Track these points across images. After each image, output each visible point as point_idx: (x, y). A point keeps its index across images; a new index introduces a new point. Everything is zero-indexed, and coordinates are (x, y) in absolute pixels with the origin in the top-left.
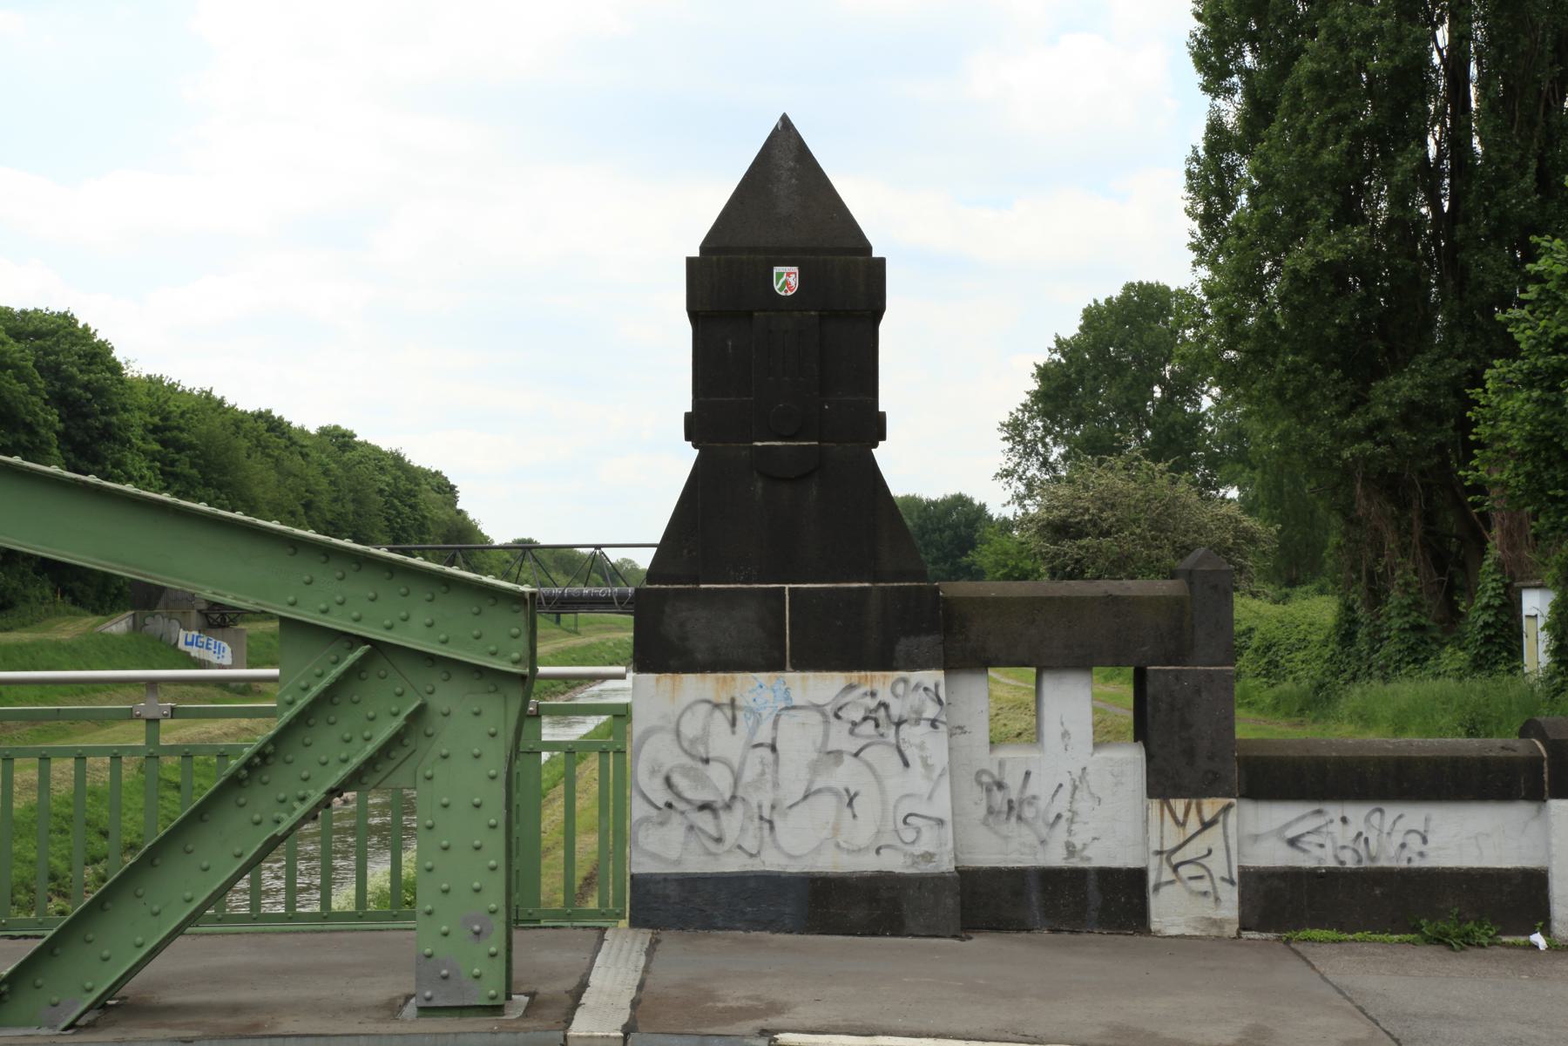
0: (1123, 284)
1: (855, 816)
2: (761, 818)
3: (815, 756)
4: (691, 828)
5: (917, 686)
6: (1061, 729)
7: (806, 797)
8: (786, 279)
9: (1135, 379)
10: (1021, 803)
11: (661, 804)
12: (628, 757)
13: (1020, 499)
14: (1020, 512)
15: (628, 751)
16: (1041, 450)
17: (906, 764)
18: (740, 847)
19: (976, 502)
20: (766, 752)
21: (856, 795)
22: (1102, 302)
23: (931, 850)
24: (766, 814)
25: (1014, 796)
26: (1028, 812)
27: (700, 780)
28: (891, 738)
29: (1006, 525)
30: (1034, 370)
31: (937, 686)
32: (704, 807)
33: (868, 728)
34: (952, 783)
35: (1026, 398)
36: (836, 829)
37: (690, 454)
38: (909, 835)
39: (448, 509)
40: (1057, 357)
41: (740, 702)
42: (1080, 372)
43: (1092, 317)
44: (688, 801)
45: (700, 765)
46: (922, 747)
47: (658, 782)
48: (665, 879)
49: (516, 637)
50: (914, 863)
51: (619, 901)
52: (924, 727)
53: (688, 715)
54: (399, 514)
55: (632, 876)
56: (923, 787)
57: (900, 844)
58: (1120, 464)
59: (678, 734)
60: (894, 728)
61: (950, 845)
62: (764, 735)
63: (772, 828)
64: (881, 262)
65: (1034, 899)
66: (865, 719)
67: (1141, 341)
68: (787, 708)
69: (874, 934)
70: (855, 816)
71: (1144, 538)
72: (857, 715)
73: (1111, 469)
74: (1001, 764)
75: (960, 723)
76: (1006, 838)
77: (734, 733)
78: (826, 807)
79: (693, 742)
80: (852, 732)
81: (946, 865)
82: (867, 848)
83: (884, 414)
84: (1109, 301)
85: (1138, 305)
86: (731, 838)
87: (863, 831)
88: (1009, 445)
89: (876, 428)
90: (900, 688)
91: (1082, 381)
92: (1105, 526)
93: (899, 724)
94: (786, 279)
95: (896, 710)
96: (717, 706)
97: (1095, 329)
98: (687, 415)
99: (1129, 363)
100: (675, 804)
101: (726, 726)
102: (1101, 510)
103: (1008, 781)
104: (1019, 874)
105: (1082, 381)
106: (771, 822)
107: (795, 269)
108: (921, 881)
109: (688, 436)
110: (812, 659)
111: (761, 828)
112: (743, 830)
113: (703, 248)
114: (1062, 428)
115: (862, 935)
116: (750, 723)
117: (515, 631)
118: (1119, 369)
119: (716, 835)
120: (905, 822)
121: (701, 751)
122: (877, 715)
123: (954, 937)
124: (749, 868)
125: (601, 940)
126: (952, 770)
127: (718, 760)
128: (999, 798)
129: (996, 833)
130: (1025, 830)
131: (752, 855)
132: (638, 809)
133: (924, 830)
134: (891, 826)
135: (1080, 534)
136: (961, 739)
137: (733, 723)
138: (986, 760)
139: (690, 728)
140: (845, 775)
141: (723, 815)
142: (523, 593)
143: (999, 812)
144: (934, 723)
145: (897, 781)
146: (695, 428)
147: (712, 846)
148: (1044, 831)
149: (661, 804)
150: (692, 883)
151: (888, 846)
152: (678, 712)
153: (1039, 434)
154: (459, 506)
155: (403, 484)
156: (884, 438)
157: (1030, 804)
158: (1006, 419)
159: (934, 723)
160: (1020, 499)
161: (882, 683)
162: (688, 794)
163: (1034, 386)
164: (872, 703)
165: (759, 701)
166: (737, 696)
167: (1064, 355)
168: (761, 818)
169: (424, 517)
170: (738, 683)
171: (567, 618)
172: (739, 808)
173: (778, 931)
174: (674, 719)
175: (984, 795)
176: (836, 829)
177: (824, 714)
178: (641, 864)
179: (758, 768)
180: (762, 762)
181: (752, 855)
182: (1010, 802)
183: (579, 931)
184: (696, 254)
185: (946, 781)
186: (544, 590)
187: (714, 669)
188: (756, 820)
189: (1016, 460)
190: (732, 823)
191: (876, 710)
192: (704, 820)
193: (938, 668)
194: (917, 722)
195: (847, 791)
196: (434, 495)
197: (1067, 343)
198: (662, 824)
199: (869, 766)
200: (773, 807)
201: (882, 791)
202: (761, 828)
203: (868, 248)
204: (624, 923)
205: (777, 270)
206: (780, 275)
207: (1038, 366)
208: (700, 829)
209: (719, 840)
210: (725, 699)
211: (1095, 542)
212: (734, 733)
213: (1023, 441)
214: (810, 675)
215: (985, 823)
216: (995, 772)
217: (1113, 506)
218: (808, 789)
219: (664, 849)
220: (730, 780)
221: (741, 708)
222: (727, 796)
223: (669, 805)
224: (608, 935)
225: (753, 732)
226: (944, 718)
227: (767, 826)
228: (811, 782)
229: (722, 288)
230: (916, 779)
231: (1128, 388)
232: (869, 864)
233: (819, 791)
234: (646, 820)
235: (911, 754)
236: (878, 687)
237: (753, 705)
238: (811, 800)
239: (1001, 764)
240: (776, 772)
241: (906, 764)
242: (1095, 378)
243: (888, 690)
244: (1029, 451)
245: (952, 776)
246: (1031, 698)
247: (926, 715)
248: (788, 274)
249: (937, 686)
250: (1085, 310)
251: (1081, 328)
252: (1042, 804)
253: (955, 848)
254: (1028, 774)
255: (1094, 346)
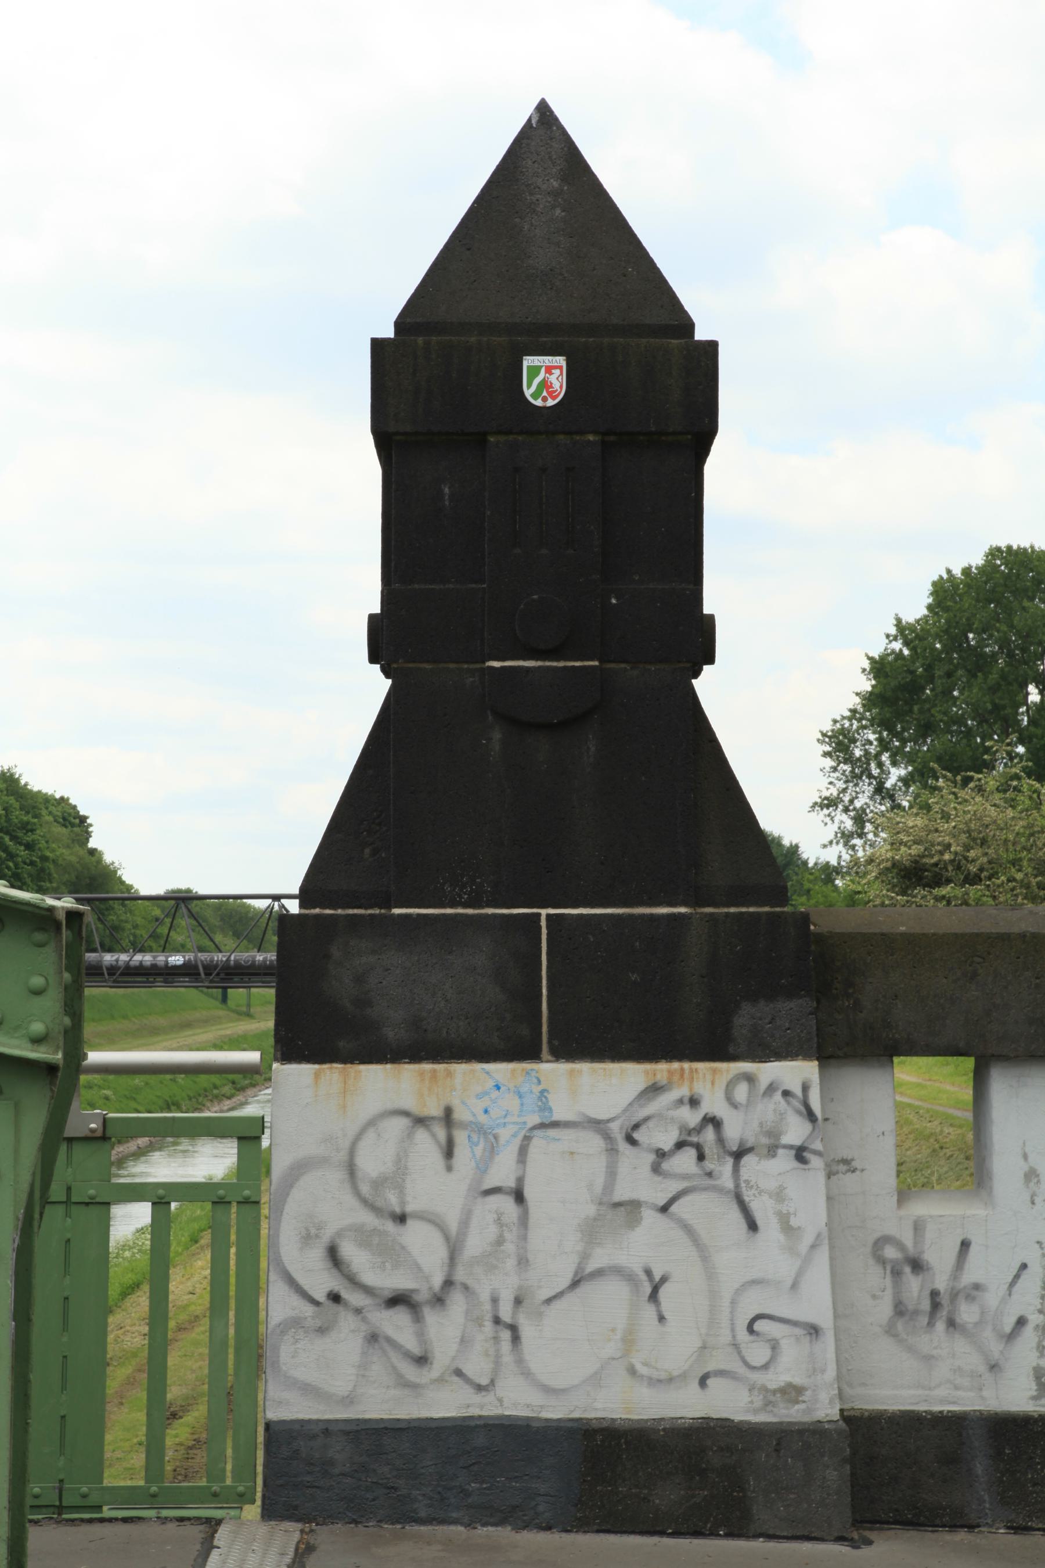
0: (986, 549)
1: (661, 1318)
2: (497, 1321)
3: (591, 1210)
4: (373, 1338)
5: (771, 1089)
6: (1023, 1167)
7: (575, 1284)
8: (545, 379)
9: (1003, 676)
10: (954, 1295)
11: (320, 1296)
12: (265, 1211)
13: (846, 837)
14: (846, 857)
15: (264, 1199)
16: (875, 772)
17: (753, 1226)
18: (459, 1373)
19: (786, 842)
20: (506, 1204)
21: (664, 1279)
22: (957, 572)
23: (798, 1380)
24: (506, 1315)
25: (941, 1283)
26: (967, 1314)
27: (391, 1254)
28: (726, 1180)
29: (828, 872)
30: (866, 664)
31: (805, 1088)
32: (397, 1300)
33: (685, 1161)
34: (832, 1259)
35: (855, 702)
36: (629, 1341)
37: (376, 686)
38: (758, 1354)
39: (77, 848)
40: (897, 646)
41: (461, 1114)
42: (929, 668)
43: (945, 592)
44: (368, 1290)
45: (390, 1226)
46: (779, 1195)
47: (317, 1255)
48: (327, 1429)
49: (38, 992)
50: (767, 1404)
51: (245, 1469)
52: (784, 1161)
53: (371, 1134)
54: (11, 856)
55: (268, 1426)
56: (784, 1268)
57: (741, 1370)
58: (992, 784)
59: (351, 1170)
60: (730, 1162)
61: (831, 1373)
62: (503, 1173)
63: (516, 1338)
64: (711, 348)
65: (979, 1469)
66: (680, 1145)
67: (1012, 626)
68: (542, 1126)
69: (697, 1534)
70: (661, 1318)
71: (1028, 886)
72: (666, 1140)
73: (980, 790)
74: (918, 1227)
75: (846, 1154)
76: (928, 1359)
77: (449, 1168)
78: (611, 1300)
79: (378, 1184)
80: (656, 1169)
81: (824, 1408)
82: (684, 1376)
83: (711, 618)
84: (966, 571)
85: (1007, 577)
86: (443, 1356)
87: (675, 1346)
88: (829, 763)
89: (698, 643)
90: (741, 1092)
91: (931, 679)
92: (973, 869)
93: (738, 1155)
94: (545, 379)
95: (734, 1131)
96: (420, 1121)
97: (947, 609)
98: (372, 618)
99: (994, 656)
100: (344, 1294)
101: (434, 1156)
102: (967, 848)
103: (930, 1256)
104: (951, 1426)
105: (931, 679)
106: (513, 1328)
107: (561, 361)
108: (780, 1437)
109: (374, 657)
110: (586, 1039)
111: (496, 1339)
112: (464, 1341)
113: (400, 325)
114: (904, 742)
115: (677, 1534)
116: (479, 1150)
117: (37, 981)
118: (978, 663)
119: (417, 1351)
120: (750, 1329)
121: (392, 1200)
122: (702, 1138)
123: (840, 1539)
124: (475, 1412)
125: (208, 1545)
126: (835, 1234)
127: (421, 1216)
128: (914, 1286)
129: (910, 1349)
130: (961, 1344)
131: (479, 1388)
132: (279, 1305)
133: (784, 1343)
134: (725, 1337)
135: (938, 881)
136: (848, 1182)
137: (449, 1152)
138: (888, 1217)
139: (373, 1161)
140: (644, 1245)
141: (430, 1316)
142: (51, 909)
143: (916, 1312)
144: (800, 1154)
145: (736, 1258)
146: (385, 641)
147: (410, 1371)
148: (995, 1347)
149: (320, 1296)
150: (373, 1438)
151: (721, 1373)
152: (352, 1130)
153: (872, 750)
154: (92, 844)
155: (18, 816)
156: (711, 660)
157: (970, 1298)
158: (828, 727)
159: (800, 1154)
160: (846, 837)
161: (710, 1082)
162: (369, 1278)
163: (866, 685)
164: (692, 1118)
165: (494, 1112)
166: (456, 1103)
167: (906, 643)
168: (497, 1321)
169: (44, 859)
170: (458, 1080)
171: (237, 994)
172: (457, 1302)
173: (526, 1526)
174: (345, 1144)
175: (888, 1281)
176: (629, 1341)
177: (608, 1137)
178: (284, 1404)
179: (493, 1231)
180: (499, 1222)
181: (479, 1388)
182: (934, 1294)
183: (171, 1526)
184: (389, 332)
185: (822, 1257)
186: (203, 956)
187: (415, 1057)
188: (489, 1326)
189: (841, 785)
190: (445, 1330)
191: (699, 1129)
192: (396, 1325)
193: (807, 1057)
194: (772, 1151)
195: (648, 1273)
196: (58, 830)
197: (911, 627)
198: (322, 1331)
199: (688, 1229)
200: (518, 1301)
201: (710, 1274)
202: (496, 1339)
203: (687, 326)
204: (252, 1511)
205: (528, 361)
206: (534, 371)
207: (871, 659)
208: (389, 1340)
209: (422, 1360)
210: (434, 1110)
211: (959, 892)
212: (449, 1168)
213: (849, 759)
214: (585, 1068)
215: (890, 1330)
216: (909, 1243)
217: (984, 842)
218: (579, 1269)
219: (325, 1376)
220: (441, 1253)
221: (464, 1126)
222: (437, 1281)
223: (335, 1298)
224: (222, 1536)
225: (483, 1168)
226: (817, 1145)
227: (506, 1335)
228: (585, 1256)
229: (431, 389)
230: (770, 1253)
231: (994, 689)
232: (687, 1404)
233: (599, 1273)
234: (295, 1323)
235: (761, 1207)
236: (701, 1088)
237: (482, 1118)
238: (585, 1288)
239: (918, 1227)
240: (524, 1238)
241: (753, 1226)
242: (949, 675)
243: (720, 1094)
244: (859, 770)
245: (832, 1248)
246: (969, 1116)
247: (786, 1140)
248: (549, 370)
249: (805, 1088)
250: (934, 584)
251: (930, 607)
252: (992, 1298)
253: (839, 1377)
254: (965, 1245)
255: (946, 632)
